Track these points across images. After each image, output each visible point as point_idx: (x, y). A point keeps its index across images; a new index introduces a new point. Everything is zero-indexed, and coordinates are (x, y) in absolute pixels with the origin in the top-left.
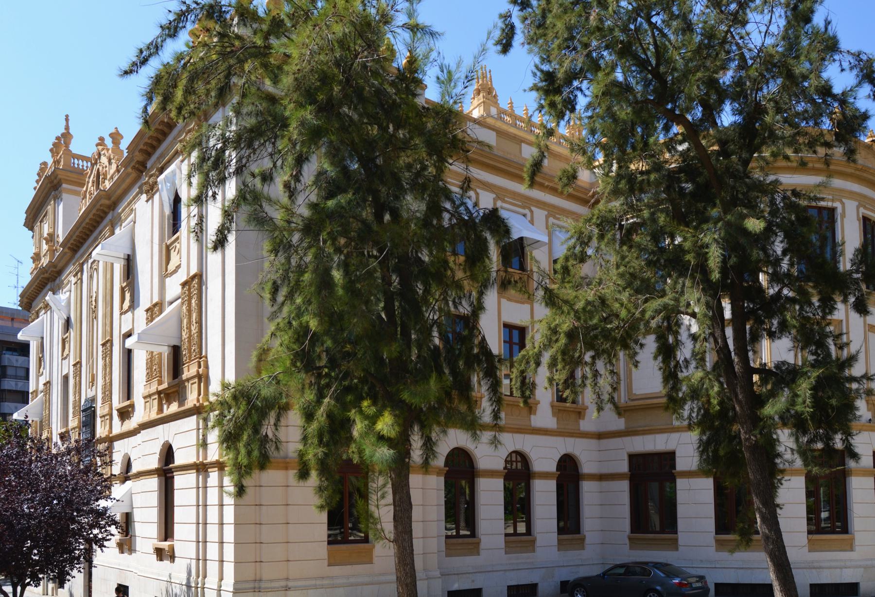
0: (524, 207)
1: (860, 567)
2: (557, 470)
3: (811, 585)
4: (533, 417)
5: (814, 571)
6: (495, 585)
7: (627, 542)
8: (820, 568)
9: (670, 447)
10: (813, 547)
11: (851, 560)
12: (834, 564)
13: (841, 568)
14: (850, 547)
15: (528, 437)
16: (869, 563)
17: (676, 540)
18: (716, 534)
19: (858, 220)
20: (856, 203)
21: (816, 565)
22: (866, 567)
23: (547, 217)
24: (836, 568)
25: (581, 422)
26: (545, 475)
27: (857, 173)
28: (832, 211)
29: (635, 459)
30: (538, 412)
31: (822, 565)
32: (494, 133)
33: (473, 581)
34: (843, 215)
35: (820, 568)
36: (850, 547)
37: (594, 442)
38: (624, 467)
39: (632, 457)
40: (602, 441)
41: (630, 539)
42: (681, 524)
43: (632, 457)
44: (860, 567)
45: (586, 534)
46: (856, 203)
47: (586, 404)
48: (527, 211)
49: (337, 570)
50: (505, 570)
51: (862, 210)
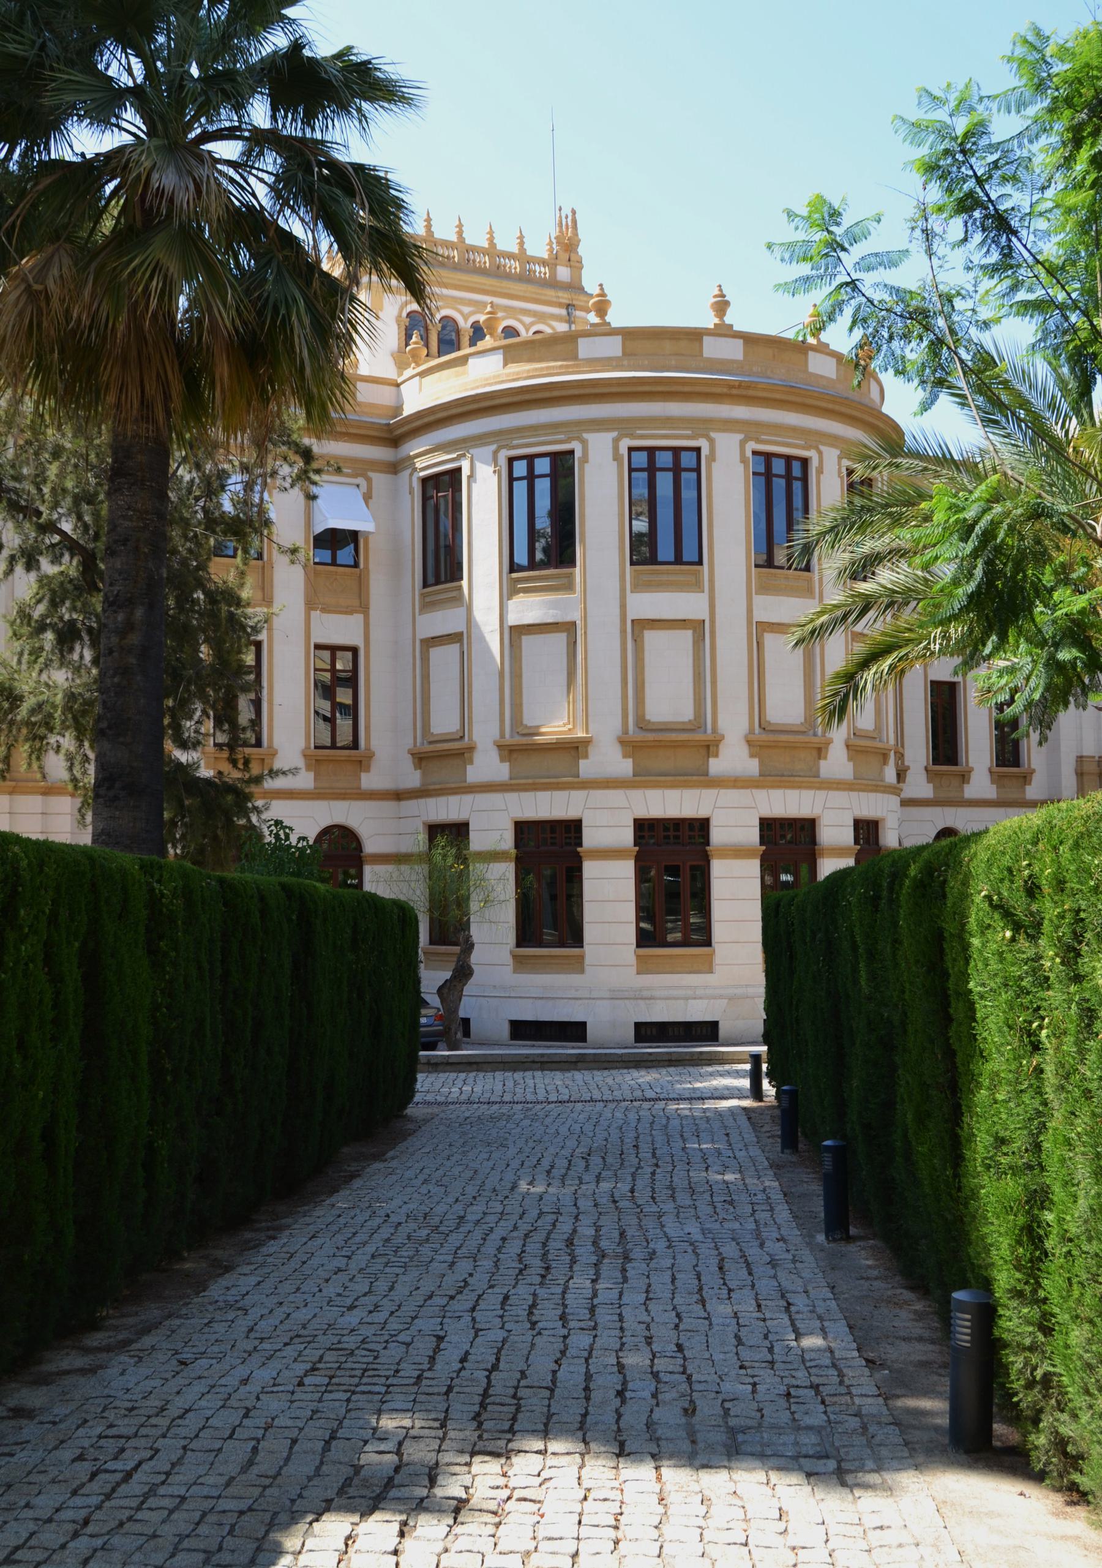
0: (355, 476)
1: (721, 997)
2: (761, 844)
3: (638, 1025)
4: (822, 763)
7: (509, 960)
9: (571, 814)
10: (520, 964)
12: (675, 993)
13: (687, 999)
14: (708, 967)
15: (468, 798)
16: (739, 991)
17: (582, 958)
18: (639, 946)
20: (838, 452)
21: (645, 994)
22: (731, 999)
23: (840, 458)
26: (738, 852)
28: (805, 462)
29: (644, 828)
30: (829, 756)
31: (657, 994)
32: (741, 341)
34: (820, 471)
36: (708, 967)
37: (389, 806)
40: (403, 803)
41: (515, 957)
42: (590, 932)
44: (721, 997)
47: (1033, 766)
48: (360, 480)
51: (846, 463)
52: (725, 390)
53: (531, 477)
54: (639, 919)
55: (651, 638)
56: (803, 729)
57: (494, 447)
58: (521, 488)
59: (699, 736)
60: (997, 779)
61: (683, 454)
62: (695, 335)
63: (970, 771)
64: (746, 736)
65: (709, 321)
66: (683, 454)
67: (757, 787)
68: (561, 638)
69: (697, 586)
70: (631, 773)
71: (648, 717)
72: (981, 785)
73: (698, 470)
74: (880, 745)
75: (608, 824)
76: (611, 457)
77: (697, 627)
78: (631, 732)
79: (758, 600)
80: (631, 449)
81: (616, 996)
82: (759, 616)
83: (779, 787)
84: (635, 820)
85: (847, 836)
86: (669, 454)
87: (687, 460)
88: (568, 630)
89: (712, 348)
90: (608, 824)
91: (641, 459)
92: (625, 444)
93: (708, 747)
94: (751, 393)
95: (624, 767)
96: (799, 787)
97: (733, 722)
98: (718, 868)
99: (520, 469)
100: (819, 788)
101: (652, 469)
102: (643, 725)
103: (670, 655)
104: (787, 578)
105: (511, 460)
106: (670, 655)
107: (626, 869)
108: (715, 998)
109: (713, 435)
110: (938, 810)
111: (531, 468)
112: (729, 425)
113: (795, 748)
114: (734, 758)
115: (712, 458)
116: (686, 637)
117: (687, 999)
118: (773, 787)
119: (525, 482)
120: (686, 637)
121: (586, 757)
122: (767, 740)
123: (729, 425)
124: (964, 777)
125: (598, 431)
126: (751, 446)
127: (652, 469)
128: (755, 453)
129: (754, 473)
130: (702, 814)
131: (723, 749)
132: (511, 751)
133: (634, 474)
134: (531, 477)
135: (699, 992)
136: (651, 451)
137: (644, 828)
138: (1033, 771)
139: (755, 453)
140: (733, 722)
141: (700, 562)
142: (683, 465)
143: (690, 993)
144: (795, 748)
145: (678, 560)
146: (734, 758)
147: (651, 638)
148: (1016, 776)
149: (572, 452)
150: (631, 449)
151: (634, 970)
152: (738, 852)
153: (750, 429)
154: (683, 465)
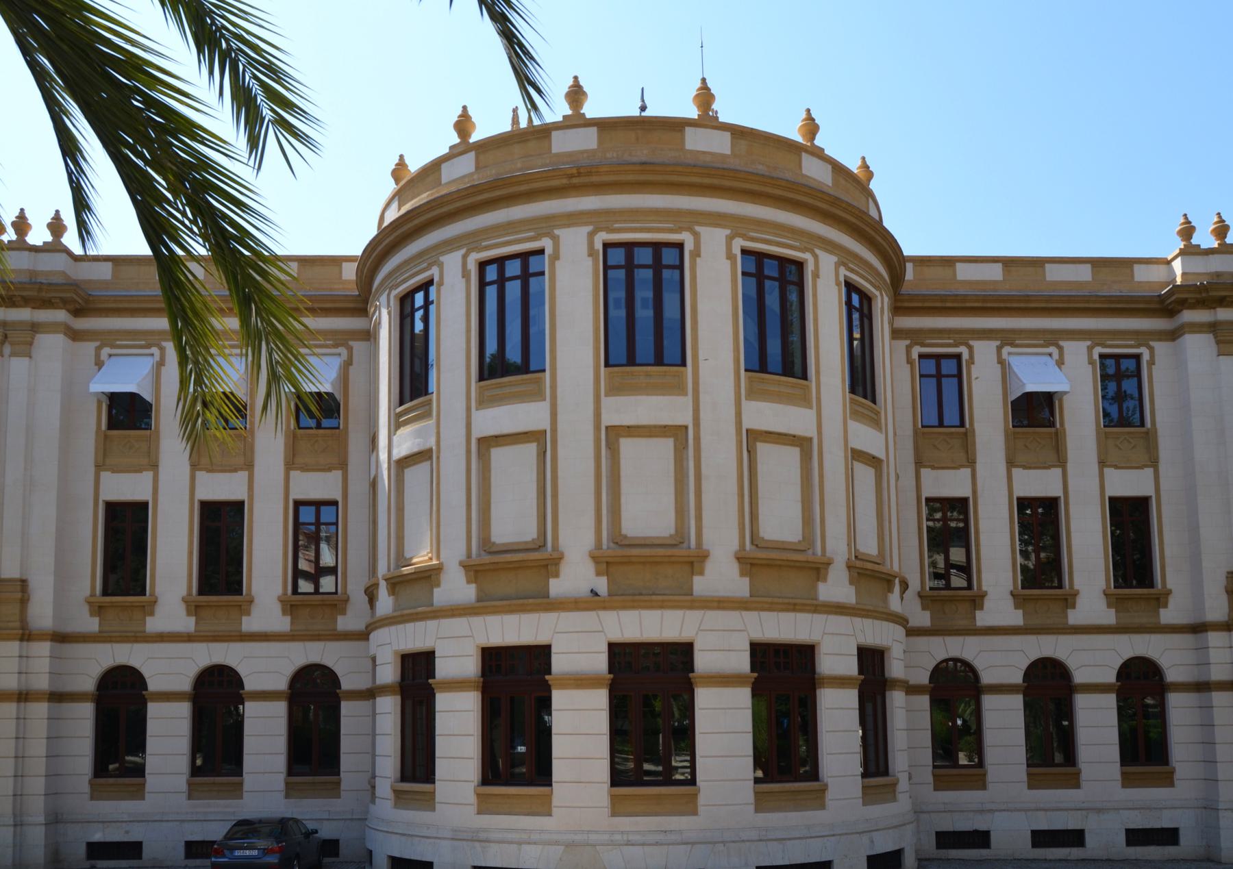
1: (557, 843)
2: (753, 670)
5: (477, 844)
6: (162, 841)
7: (473, 799)
8: (487, 841)
11: (542, 831)
12: (510, 836)
13: (520, 843)
14: (545, 809)
16: (578, 837)
19: (838, 284)
21: (483, 836)
22: (570, 845)
24: (511, 843)
25: (1162, 611)
26: (581, 681)
27: (575, 181)
28: (800, 265)
29: (619, 653)
33: (127, 832)
34: (816, 275)
35: (487, 841)
36: (545, 809)
38: (600, 663)
39: (615, 650)
43: (615, 650)
44: (557, 843)
45: (830, 781)
46: (834, 259)
47: (1169, 586)
49: (625, 823)
50: (183, 821)
51: (843, 272)
52: (565, 181)
53: (502, 281)
54: (934, 759)
55: (764, 450)
56: (674, 542)
57: (463, 251)
58: (492, 292)
59: (808, 556)
60: (1113, 601)
61: (665, 251)
62: (676, 126)
63: (1075, 594)
64: (736, 553)
65: (692, 113)
66: (665, 251)
67: (746, 609)
68: (531, 449)
69: (680, 389)
70: (748, 595)
71: (624, 532)
72: (999, 606)
73: (681, 267)
74: (810, 558)
75: (579, 646)
76: (724, 256)
77: (677, 433)
78: (605, 547)
79: (607, 402)
80: (606, 246)
81: (458, 836)
82: (608, 419)
83: (633, 608)
84: (612, 646)
85: (849, 666)
86: (649, 250)
87: (669, 257)
88: (537, 440)
89: (695, 141)
90: (579, 646)
91: (618, 256)
92: (474, 258)
93: (692, 563)
94: (595, 179)
95: (740, 586)
96: (662, 607)
97: (721, 538)
98: (704, 698)
99: (492, 273)
100: (691, 608)
101: (630, 267)
102: (619, 540)
103: (646, 464)
104: (648, 375)
105: (483, 265)
106: (646, 464)
107: (600, 699)
108: (550, 843)
109: (698, 228)
110: (1032, 639)
111: (501, 271)
112: (573, 219)
113: (657, 563)
114: (722, 575)
115: (696, 253)
116: (666, 446)
117: (520, 843)
118: (624, 608)
119: (518, 282)
120: (666, 446)
121: (557, 575)
122: (759, 561)
123: (573, 219)
124: (1069, 601)
125: (569, 226)
126: (602, 237)
127: (630, 267)
128: (745, 252)
129: (744, 274)
130: (541, 640)
131: (710, 566)
132: (476, 572)
133: (610, 272)
134: (502, 281)
135: (535, 837)
136: (629, 246)
137: (619, 653)
138: (1169, 593)
139: (745, 252)
140: (721, 538)
141: (684, 364)
142: (664, 262)
143: (524, 836)
144: (657, 563)
145: (659, 361)
146: (722, 575)
147: (764, 450)
148: (1147, 599)
149: (541, 252)
150: (606, 246)
151: (474, 809)
152: (581, 681)
153: (737, 225)
154: (664, 262)
